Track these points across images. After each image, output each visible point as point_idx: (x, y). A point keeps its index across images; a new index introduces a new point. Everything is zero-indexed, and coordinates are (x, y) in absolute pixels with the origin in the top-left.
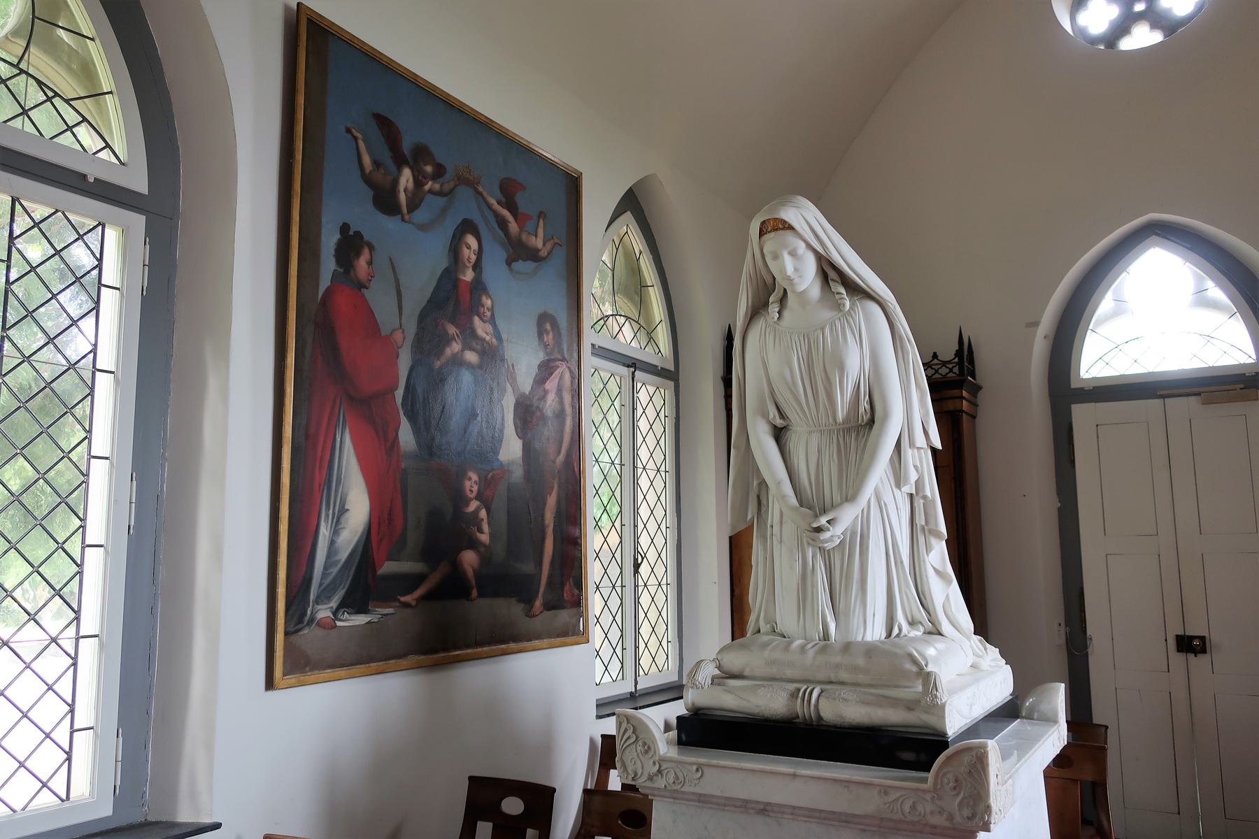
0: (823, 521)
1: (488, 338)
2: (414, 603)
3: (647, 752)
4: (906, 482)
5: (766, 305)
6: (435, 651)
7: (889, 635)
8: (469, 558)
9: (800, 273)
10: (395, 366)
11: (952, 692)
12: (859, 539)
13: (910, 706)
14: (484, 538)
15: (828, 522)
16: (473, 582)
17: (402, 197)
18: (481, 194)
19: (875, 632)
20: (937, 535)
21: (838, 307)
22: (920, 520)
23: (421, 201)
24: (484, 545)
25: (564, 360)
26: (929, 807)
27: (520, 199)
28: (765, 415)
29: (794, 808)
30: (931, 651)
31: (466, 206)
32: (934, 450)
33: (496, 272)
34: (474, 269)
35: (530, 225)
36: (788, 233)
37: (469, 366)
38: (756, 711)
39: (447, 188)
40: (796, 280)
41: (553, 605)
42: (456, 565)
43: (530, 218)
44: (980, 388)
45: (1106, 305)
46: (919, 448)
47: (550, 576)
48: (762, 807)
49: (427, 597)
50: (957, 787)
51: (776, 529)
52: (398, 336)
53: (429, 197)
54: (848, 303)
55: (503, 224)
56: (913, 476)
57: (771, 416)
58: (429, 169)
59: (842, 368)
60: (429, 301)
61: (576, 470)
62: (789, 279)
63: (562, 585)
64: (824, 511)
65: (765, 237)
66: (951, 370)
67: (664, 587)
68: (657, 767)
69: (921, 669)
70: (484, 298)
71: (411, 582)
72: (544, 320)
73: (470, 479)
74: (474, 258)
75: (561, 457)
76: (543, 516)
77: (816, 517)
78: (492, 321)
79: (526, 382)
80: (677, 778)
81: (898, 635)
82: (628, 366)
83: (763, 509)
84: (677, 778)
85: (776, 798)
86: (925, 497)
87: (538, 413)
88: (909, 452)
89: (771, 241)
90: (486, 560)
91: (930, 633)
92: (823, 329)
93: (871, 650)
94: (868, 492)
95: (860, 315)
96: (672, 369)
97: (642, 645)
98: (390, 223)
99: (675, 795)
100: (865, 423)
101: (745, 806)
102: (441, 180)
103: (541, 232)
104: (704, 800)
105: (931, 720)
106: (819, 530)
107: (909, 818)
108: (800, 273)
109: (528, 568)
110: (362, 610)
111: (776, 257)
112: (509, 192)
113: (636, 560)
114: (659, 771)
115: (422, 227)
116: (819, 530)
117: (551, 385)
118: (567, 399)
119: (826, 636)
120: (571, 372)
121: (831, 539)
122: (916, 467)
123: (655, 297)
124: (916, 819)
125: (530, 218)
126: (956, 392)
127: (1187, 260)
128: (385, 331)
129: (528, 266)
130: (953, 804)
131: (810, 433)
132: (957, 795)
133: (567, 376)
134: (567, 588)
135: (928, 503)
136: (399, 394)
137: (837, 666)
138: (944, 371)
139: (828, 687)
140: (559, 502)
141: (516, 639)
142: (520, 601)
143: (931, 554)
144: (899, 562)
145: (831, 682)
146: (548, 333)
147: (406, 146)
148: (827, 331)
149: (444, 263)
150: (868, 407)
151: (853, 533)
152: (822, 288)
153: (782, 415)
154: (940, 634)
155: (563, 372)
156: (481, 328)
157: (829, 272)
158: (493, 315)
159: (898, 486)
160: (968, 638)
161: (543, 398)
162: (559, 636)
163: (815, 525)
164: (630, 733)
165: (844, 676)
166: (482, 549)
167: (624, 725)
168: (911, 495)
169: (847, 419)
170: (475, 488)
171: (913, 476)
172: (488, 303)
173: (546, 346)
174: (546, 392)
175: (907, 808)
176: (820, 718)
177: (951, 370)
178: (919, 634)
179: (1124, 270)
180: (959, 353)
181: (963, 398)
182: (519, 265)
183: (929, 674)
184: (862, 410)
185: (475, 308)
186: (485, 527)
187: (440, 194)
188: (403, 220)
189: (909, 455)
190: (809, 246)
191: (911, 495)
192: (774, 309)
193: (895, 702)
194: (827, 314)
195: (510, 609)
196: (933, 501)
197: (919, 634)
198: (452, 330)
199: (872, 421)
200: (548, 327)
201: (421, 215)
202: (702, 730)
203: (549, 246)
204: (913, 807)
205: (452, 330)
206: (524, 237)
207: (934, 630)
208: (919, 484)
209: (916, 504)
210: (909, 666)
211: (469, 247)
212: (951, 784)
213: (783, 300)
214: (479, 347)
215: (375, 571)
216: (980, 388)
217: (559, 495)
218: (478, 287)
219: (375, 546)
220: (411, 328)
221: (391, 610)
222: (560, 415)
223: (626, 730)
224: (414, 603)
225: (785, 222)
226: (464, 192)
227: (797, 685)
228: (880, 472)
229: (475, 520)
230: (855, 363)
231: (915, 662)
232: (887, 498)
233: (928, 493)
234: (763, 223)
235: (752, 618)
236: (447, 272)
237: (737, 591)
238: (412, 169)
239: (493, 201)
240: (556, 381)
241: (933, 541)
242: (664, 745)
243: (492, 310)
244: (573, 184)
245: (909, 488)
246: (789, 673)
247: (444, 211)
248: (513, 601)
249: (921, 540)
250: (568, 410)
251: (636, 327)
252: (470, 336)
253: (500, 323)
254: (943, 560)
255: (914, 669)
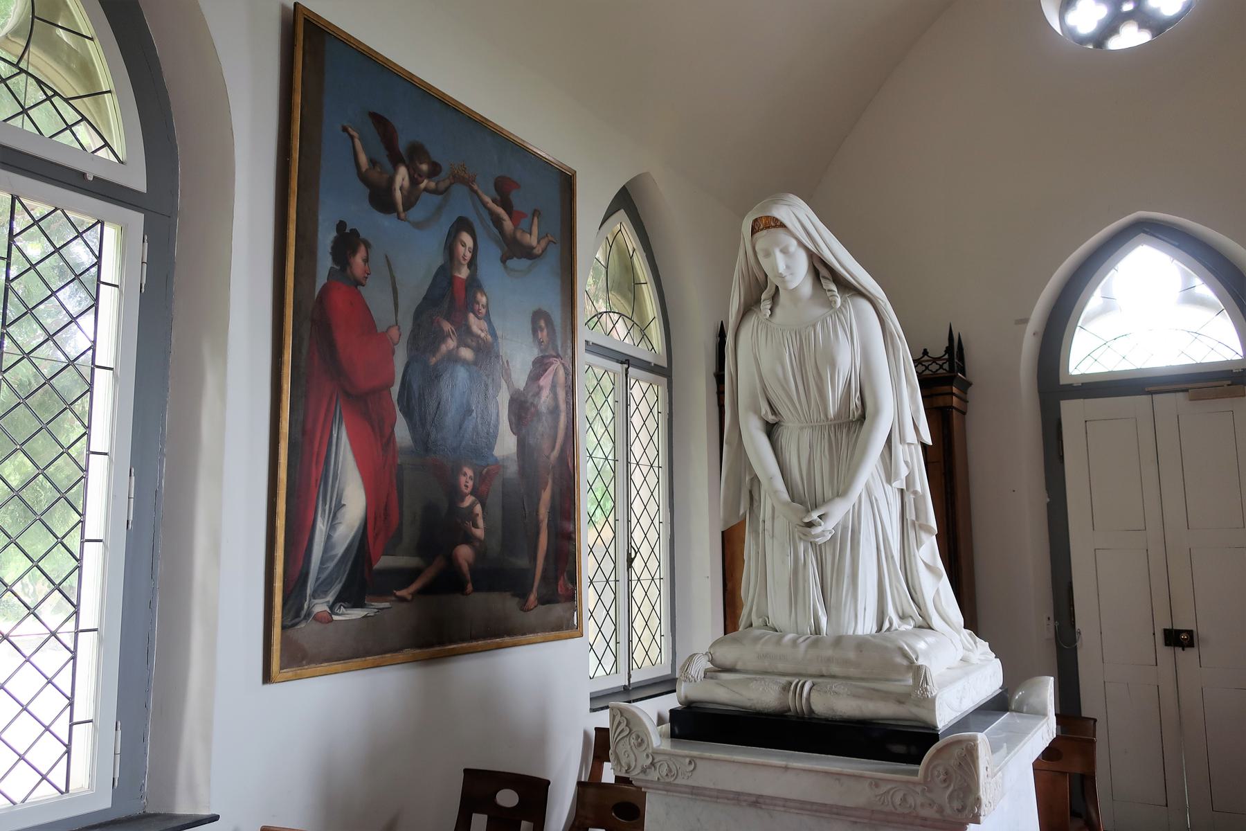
0: (815, 516)
1: (483, 335)
2: (409, 597)
3: (640, 745)
4: (897, 477)
5: (758, 302)
6: (431, 645)
7: (880, 629)
8: (464, 553)
9: (792, 270)
10: (391, 362)
11: (942, 686)
12: (850, 534)
13: (901, 699)
14: (479, 533)
15: (820, 517)
16: (469, 576)
17: (398, 195)
18: (476, 192)
19: (866, 626)
20: (928, 530)
21: (830, 304)
22: (910, 515)
23: (417, 199)
24: (479, 540)
25: (558, 356)
26: (920, 800)
27: (515, 197)
28: (757, 411)
29: (786, 800)
30: (921, 645)
31: (461, 204)
32: (924, 446)
33: (491, 270)
34: (469, 267)
35: (524, 223)
36: (780, 230)
37: (465, 362)
38: (748, 704)
39: (442, 186)
40: (788, 278)
41: (547, 599)
42: (451, 560)
43: (525, 216)
44: (969, 384)
45: (1094, 302)
46: (909, 444)
47: (545, 571)
48: (754, 799)
49: (423, 591)
50: (947, 779)
51: (768, 524)
52: (394, 333)
53: (425, 196)
54: (839, 300)
55: (497, 221)
56: (904, 472)
57: (763, 412)
58: (424, 167)
59: (833, 364)
60: (425, 298)
61: (571, 465)
62: (781, 276)
63: (557, 579)
64: (816, 506)
65: (758, 235)
66: (941, 367)
67: (657, 582)
68: (650, 759)
69: (912, 662)
70: (479, 296)
71: (407, 576)
72: (538, 317)
73: (465, 474)
74: (469, 255)
75: (556, 453)
76: (537, 511)
77: (808, 512)
78: (487, 318)
79: (520, 379)
80: (670, 770)
81: (889, 629)
82: (622, 363)
83: (755, 504)
84: (670, 770)
85: (768, 791)
86: (915, 493)
87: (533, 409)
88: (900, 447)
89: (763, 239)
90: (481, 554)
91: (920, 627)
92: (814, 326)
93: (862, 644)
94: (859, 487)
95: (851, 312)
96: (665, 365)
97: (635, 639)
98: (386, 221)
99: (668, 788)
100: (856, 419)
101: (737, 798)
102: (436, 178)
103: (535, 230)
104: (696, 792)
105: (921, 713)
106: (810, 525)
107: (900, 810)
108: (792, 270)
109: (523, 562)
110: (358, 604)
111: (768, 254)
112: (504, 191)
113: (629, 554)
114: (653, 764)
115: (418, 225)
116: (810, 525)
117: (545, 381)
118: (561, 395)
119: (817, 630)
120: (565, 368)
121: (822, 534)
122: (906, 462)
123: (648, 294)
124: (906, 811)
125: (525, 216)
126: (946, 389)
127: (1175, 257)
128: (381, 328)
129: (523, 263)
130: (943, 796)
131: (802, 429)
132: (948, 787)
133: (561, 372)
134: (561, 582)
135: (918, 499)
136: (395, 390)
137: (829, 660)
138: (934, 367)
139: (820, 680)
140: (553, 497)
141: (510, 633)
142: (514, 595)
143: (921, 549)
144: (890, 557)
145: (822, 676)
146: (542, 330)
147: (402, 145)
148: (819, 327)
149: (439, 261)
150: (859, 403)
151: (845, 528)
152: (814, 285)
153: (774, 411)
154: (931, 628)
155: (557, 369)
156: (476, 325)
157: (820, 269)
158: (488, 312)
159: (889, 481)
160: (958, 632)
161: (538, 394)
162: (553, 630)
163: (806, 520)
164: (623, 726)
165: (835, 669)
166: (477, 544)
167: (618, 718)
168: (902, 491)
169: (838, 415)
170: (470, 484)
171: (904, 472)
172: (483, 300)
173: (540, 343)
174: (540, 389)
175: (897, 800)
176: (811, 711)
177: (941, 367)
178: (909, 628)
179: (1113, 267)
180: (949, 350)
181: (953, 394)
182: (514, 263)
183: (919, 667)
184: (853, 406)
185: (470, 305)
186: (480, 522)
187: (435, 192)
188: (399, 218)
189: (900, 450)
190: (801, 244)
191: (902, 491)
192: (766, 306)
193: (886, 696)
194: (818, 311)
195: (505, 604)
196: (924, 496)
197: (909, 628)
198: (447, 327)
199: (863, 417)
200: (542, 324)
201: (417, 213)
202: (695, 723)
203: (543, 243)
204: (904, 799)
205: (447, 327)
206: (519, 235)
207: (924, 624)
208: (909, 479)
209: (906, 499)
210: (900, 660)
211: (464, 245)
212: (942, 777)
213: (775, 297)
214: (474, 344)
215: (371, 566)
216: (969, 384)
217: (553, 490)
218: (473, 284)
219: (371, 540)
220: (407, 325)
221: (387, 605)
222: (554, 411)
223: (619, 723)
224: (409, 597)
225: (777, 220)
226: (459, 191)
227: (789, 679)
228: (871, 467)
229: (470, 515)
230: (846, 359)
231: (905, 655)
232: (878, 493)
233: (919, 489)
234: (755, 221)
235: (745, 612)
236: (442, 270)
237: (729, 586)
238: (407, 167)
239: (488, 200)
240: (551, 377)
241: (924, 536)
242: (657, 738)
243: (487, 307)
244: (567, 182)
245: (900, 483)
246: (781, 666)
247: (440, 209)
248: (508, 595)
249: (912, 534)
250: (563, 406)
251: (629, 324)
252: (465, 333)
253: (495, 320)
254: (934, 555)
255: (905, 662)
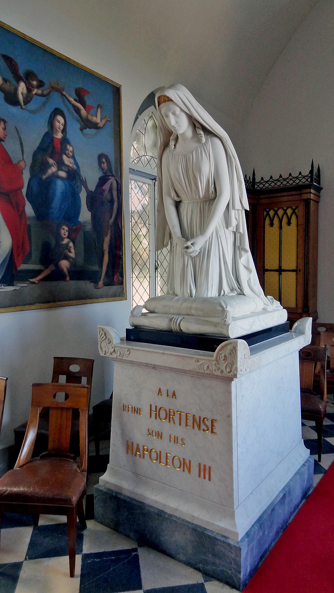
0: (189, 244)
1: (71, 165)
2: (37, 282)
3: (109, 343)
4: (231, 225)
6: (49, 302)
7: (219, 295)
8: (64, 264)
9: (183, 127)
10: (21, 178)
11: (235, 319)
12: (205, 253)
13: (216, 325)
14: (72, 255)
15: (192, 244)
16: (67, 273)
17: (21, 97)
18: (65, 96)
19: (213, 292)
20: (246, 251)
21: (199, 141)
22: (238, 244)
23: (31, 99)
24: (72, 258)
25: (113, 176)
26: (214, 368)
27: (87, 99)
28: (170, 195)
29: (165, 367)
31: (56, 101)
32: (246, 211)
33: (74, 133)
34: (62, 132)
35: (92, 111)
36: (170, 102)
37: (61, 178)
38: (156, 327)
39: (45, 92)
40: (177, 128)
41: (109, 283)
42: (57, 265)
43: (93, 108)
44: (321, 189)
47: (107, 272)
49: (44, 279)
50: (225, 358)
52: (22, 164)
53: (35, 97)
55: (77, 110)
57: (173, 196)
58: (35, 83)
59: (200, 171)
60: (38, 148)
63: (113, 275)
65: (161, 106)
66: (307, 180)
70: (68, 147)
71: (36, 273)
73: (64, 229)
74: (62, 127)
75: (112, 220)
76: (102, 246)
78: (73, 157)
80: (120, 354)
81: (223, 295)
84: (120, 354)
85: (157, 363)
86: (240, 233)
90: (73, 264)
92: (192, 153)
93: (207, 301)
98: (14, 110)
99: (122, 361)
100: (212, 198)
101: (147, 365)
102: (42, 88)
104: (132, 363)
105: (224, 332)
106: (187, 248)
107: (206, 372)
108: (183, 127)
109: (96, 268)
110: (11, 284)
111: (167, 116)
112: (80, 95)
114: (114, 351)
115: (32, 112)
116: (187, 248)
117: (106, 187)
118: (115, 193)
119: (191, 296)
121: (193, 252)
122: (236, 219)
124: (209, 372)
125: (93, 108)
126: (308, 190)
128: (15, 161)
129: (92, 131)
130: (223, 366)
131: (189, 203)
134: (115, 277)
136: (24, 191)
137: (190, 308)
138: (304, 180)
139: (186, 317)
140: (111, 240)
141: (90, 298)
142: (91, 282)
143: (242, 259)
144: (225, 263)
146: (104, 163)
147: (21, 72)
148: (194, 152)
149: (45, 129)
150: (213, 190)
151: (205, 249)
152: (193, 132)
156: (67, 160)
157: (194, 123)
159: (227, 228)
162: (111, 297)
165: (193, 312)
166: (71, 260)
169: (205, 197)
170: (67, 233)
171: (234, 223)
172: (70, 149)
173: (103, 169)
174: (104, 191)
177: (307, 180)
180: (311, 172)
181: (311, 193)
182: (87, 131)
184: (211, 192)
185: (64, 151)
186: (72, 250)
187: (42, 95)
188: (22, 108)
189: (233, 213)
190: (182, 110)
192: (172, 143)
194: (194, 145)
195: (87, 285)
196: (244, 234)
198: (51, 161)
200: (104, 160)
201: (32, 106)
203: (104, 121)
204: (208, 367)
205: (51, 161)
206: (90, 117)
207: (241, 293)
211: (59, 122)
213: (177, 139)
214: (66, 170)
215: (16, 269)
216: (321, 189)
217: (111, 236)
218: (65, 141)
219: (15, 257)
220: (29, 160)
221: (25, 285)
222: (112, 201)
224: (37, 282)
225: (168, 98)
226: (55, 96)
229: (67, 247)
230: (207, 169)
231: (222, 307)
232: (221, 233)
233: (241, 231)
236: (47, 134)
238: (25, 83)
239: (72, 100)
241: (243, 253)
243: (73, 152)
244: (116, 91)
245: (232, 228)
247: (44, 104)
248: (88, 282)
249: (238, 252)
252: (61, 164)
